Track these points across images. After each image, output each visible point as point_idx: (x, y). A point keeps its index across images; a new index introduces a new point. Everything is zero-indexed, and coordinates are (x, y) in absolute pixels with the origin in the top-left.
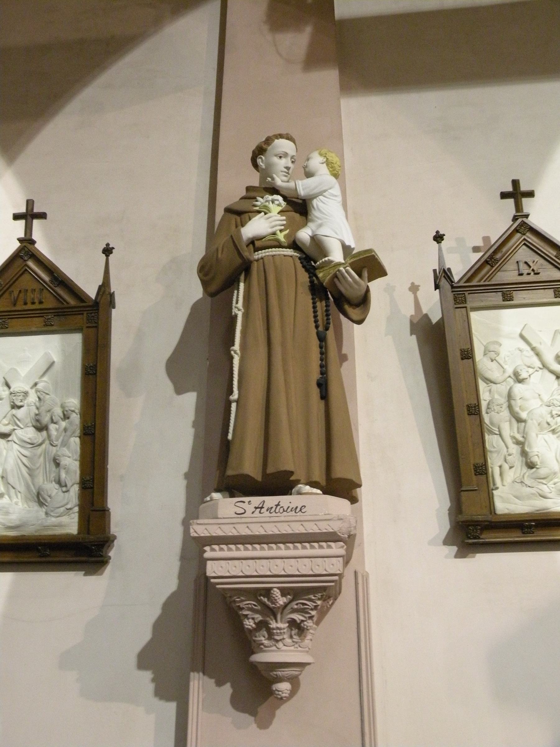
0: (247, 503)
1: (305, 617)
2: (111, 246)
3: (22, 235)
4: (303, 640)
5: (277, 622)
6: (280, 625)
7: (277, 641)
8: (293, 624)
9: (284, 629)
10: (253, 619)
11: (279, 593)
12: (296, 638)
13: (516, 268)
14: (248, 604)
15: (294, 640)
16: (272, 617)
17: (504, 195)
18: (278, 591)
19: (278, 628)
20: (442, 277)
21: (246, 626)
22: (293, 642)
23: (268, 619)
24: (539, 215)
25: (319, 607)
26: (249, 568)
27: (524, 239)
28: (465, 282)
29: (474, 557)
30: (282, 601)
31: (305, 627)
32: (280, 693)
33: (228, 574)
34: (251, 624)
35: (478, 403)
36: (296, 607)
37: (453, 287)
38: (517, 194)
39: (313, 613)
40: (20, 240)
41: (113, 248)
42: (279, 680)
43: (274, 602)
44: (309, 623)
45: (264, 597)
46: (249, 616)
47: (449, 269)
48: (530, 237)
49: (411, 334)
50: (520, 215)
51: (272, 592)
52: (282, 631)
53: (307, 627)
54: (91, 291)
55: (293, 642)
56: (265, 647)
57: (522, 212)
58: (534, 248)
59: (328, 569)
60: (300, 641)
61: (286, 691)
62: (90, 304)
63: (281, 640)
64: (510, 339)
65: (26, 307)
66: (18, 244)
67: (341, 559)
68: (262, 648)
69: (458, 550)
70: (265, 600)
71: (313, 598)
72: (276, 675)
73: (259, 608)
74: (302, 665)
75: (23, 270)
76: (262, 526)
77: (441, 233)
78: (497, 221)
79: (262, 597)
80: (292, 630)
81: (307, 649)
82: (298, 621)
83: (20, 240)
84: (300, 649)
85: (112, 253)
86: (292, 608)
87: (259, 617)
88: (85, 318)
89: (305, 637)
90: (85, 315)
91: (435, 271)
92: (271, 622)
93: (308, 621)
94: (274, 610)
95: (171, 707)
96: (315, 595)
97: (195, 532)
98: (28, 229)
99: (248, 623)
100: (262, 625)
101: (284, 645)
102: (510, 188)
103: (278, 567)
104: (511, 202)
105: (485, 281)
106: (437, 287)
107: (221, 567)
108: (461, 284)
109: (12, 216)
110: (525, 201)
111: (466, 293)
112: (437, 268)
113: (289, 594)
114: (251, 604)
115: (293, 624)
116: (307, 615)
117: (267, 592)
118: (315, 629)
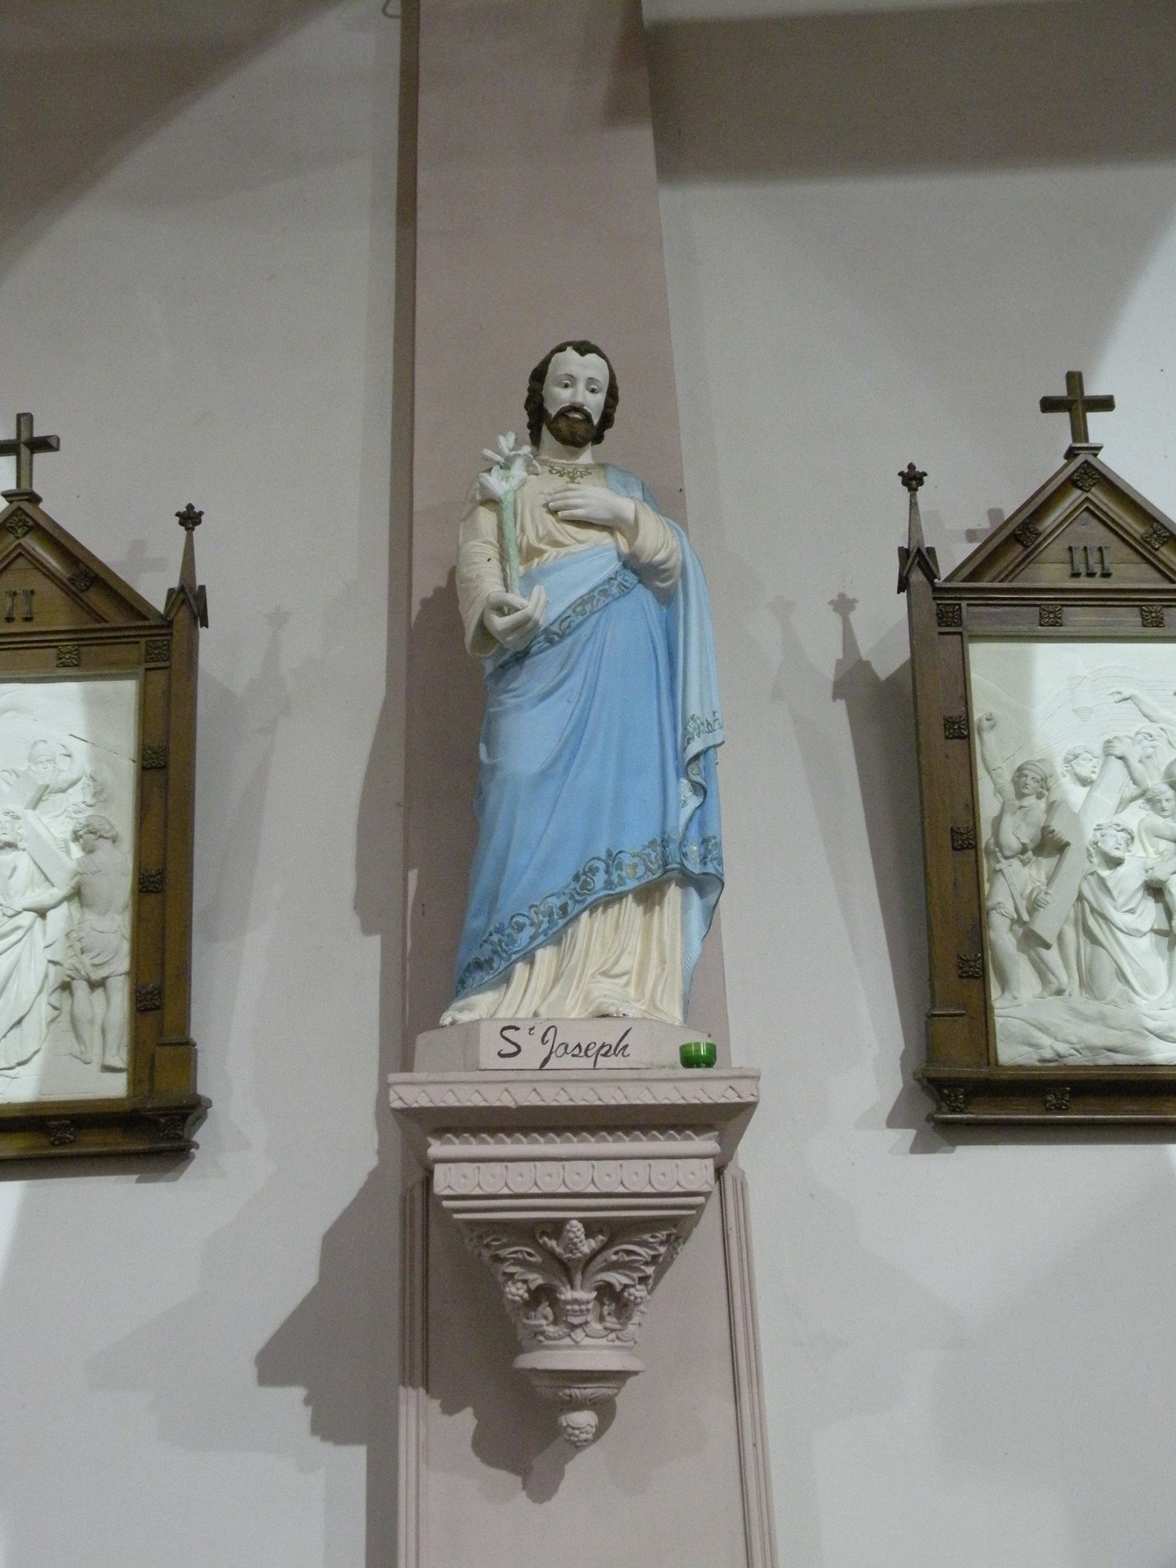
1: (633, 1280)
2: (197, 510)
3: (12, 486)
4: (624, 1325)
5: (573, 1287)
7: (573, 1327)
8: (606, 1292)
9: (588, 1302)
10: (525, 1282)
12: (611, 1322)
13: (1068, 559)
15: (608, 1325)
16: (564, 1279)
17: (1049, 405)
18: (580, 1226)
19: (575, 1301)
20: (916, 561)
21: (510, 1296)
22: (606, 1329)
23: (557, 1283)
25: (661, 1259)
26: (521, 1179)
27: (1087, 499)
28: (964, 581)
29: (952, 1151)
30: (587, 1246)
31: (632, 1298)
32: (577, 1432)
33: (478, 1192)
34: (521, 1292)
36: (614, 1258)
37: (936, 589)
39: (650, 1270)
40: (7, 495)
41: (201, 513)
42: (576, 1405)
43: (571, 1246)
44: (639, 1292)
47: (931, 551)
48: (1098, 495)
49: (835, 697)
51: (568, 1227)
52: (583, 1307)
53: (636, 1298)
55: (606, 1329)
56: (548, 1338)
57: (1087, 440)
58: (1100, 515)
59: (683, 1183)
60: (618, 1327)
61: (589, 1428)
62: (158, 622)
63: (580, 1325)
64: (1071, 708)
65: (12, 628)
68: (540, 1341)
70: (552, 1243)
71: (651, 1240)
72: (570, 1396)
73: (537, 1259)
74: (619, 1377)
76: (535, 1090)
77: (919, 469)
79: (546, 1239)
80: (602, 1304)
81: (631, 1344)
82: (618, 1288)
83: (7, 495)
84: (617, 1343)
85: (200, 522)
86: (606, 1261)
87: (536, 1279)
88: (143, 650)
89: (629, 1318)
92: (562, 1289)
93: (638, 1287)
94: (570, 1265)
95: (355, 1457)
96: (646, 1234)
97: (400, 1098)
99: (513, 1290)
100: (541, 1295)
101: (587, 1335)
102: (1060, 390)
103: (579, 1177)
104: (1062, 419)
105: (1002, 581)
107: (470, 1175)
110: (1094, 419)
111: (964, 604)
113: (601, 1232)
114: (521, 1252)
115: (606, 1292)
116: (636, 1275)
117: (557, 1228)
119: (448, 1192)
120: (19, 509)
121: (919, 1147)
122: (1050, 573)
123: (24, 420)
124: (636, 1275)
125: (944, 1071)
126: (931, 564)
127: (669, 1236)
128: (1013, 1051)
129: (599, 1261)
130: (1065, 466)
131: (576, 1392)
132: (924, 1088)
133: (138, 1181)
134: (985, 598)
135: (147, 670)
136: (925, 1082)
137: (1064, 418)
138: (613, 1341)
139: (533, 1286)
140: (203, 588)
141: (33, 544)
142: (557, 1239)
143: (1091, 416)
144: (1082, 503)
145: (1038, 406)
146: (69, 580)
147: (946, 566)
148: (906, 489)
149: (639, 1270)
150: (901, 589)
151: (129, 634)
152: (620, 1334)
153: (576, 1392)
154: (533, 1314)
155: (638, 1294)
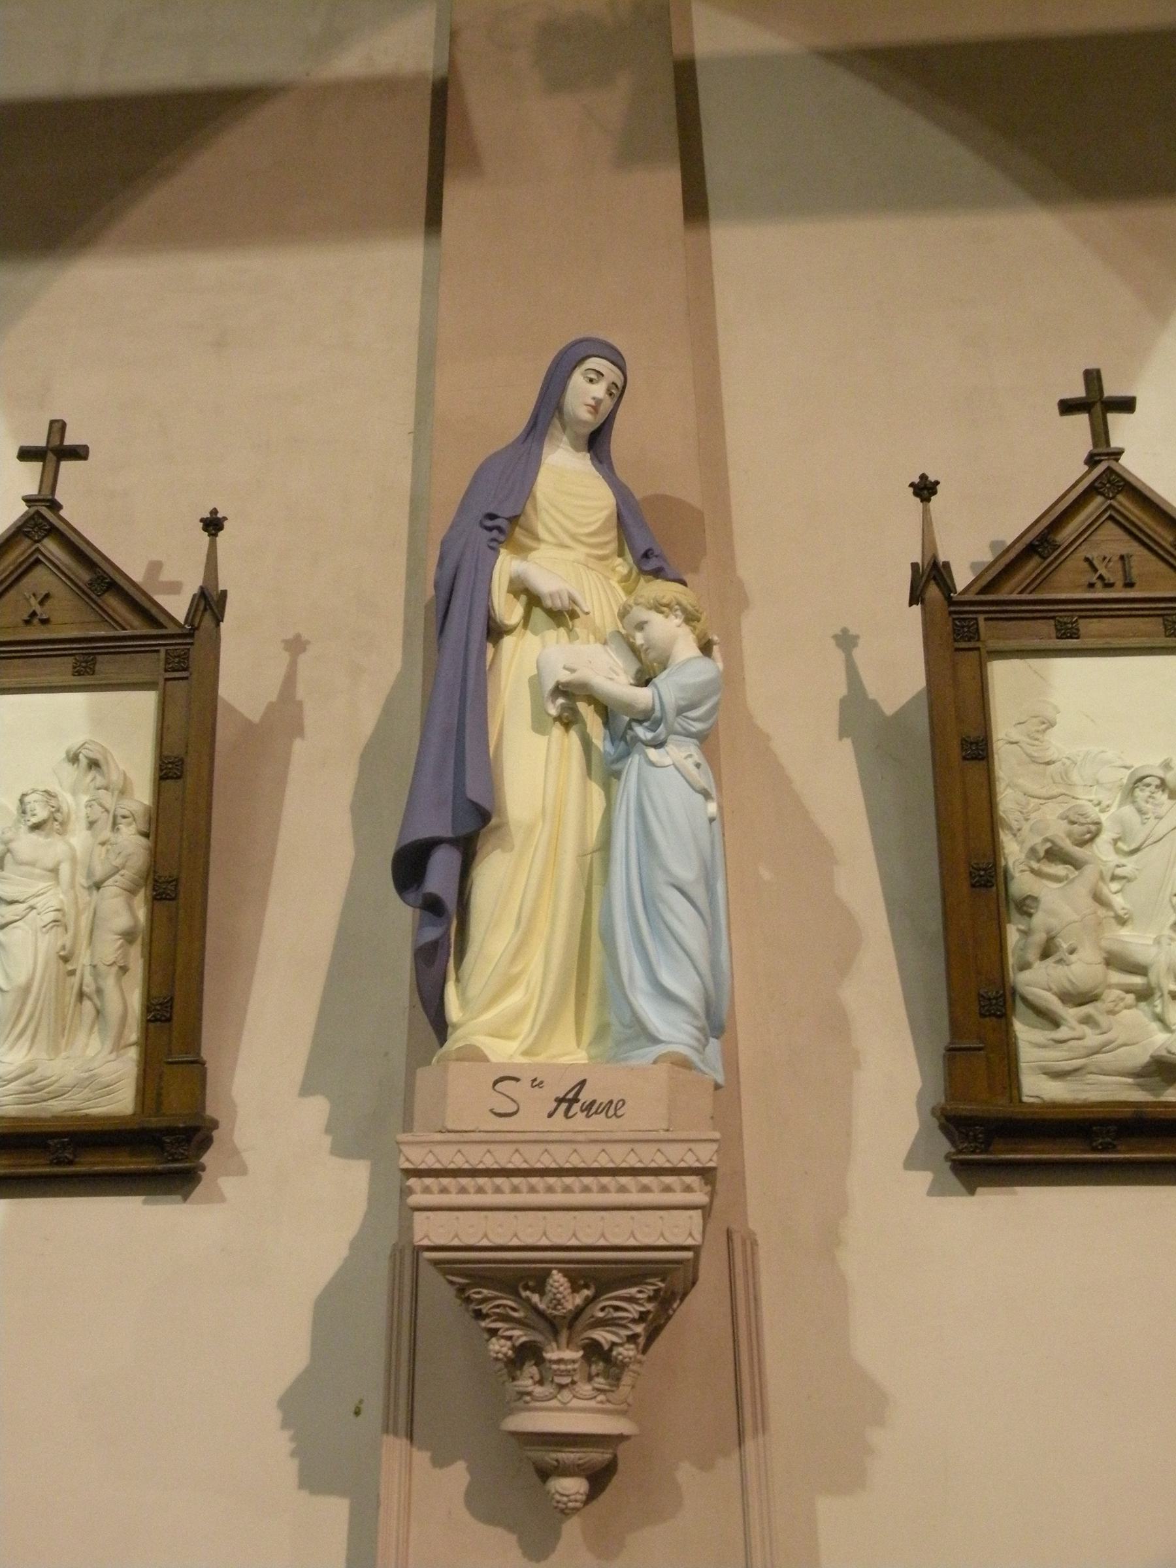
0: (526, 1083)
2: (219, 516)
3: (32, 490)
6: (568, 1354)
7: (561, 1387)
10: (510, 1338)
11: (567, 1285)
12: (600, 1382)
14: (498, 1306)
15: (597, 1386)
17: (1068, 407)
18: (563, 1280)
20: (930, 577)
24: (81, 500)
25: (651, 1316)
27: (1110, 507)
28: (978, 594)
30: (574, 1301)
31: (620, 1357)
32: (565, 1499)
34: (504, 1350)
35: (995, 859)
36: (601, 1315)
37: (951, 602)
38: (1097, 403)
39: (639, 1329)
40: (28, 500)
45: (533, 1291)
46: (500, 1333)
47: (947, 565)
50: (1102, 453)
54: (178, 607)
56: (535, 1399)
66: (23, 508)
67: (699, 1212)
69: (933, 1180)
70: (535, 1298)
72: (557, 1461)
75: (32, 560)
77: (932, 478)
78: (1056, 461)
81: (624, 1407)
82: (606, 1347)
83: (28, 500)
84: (609, 1406)
87: (521, 1336)
90: (162, 655)
91: (914, 566)
93: (627, 1346)
95: (335, 1511)
98: (50, 480)
101: (574, 1396)
105: (1021, 592)
106: (915, 598)
108: (970, 597)
109: (15, 452)
111: (981, 618)
112: (920, 562)
113: (586, 1286)
114: (505, 1306)
115: (594, 1351)
116: (625, 1333)
118: (640, 1362)
119: (426, 1242)
120: (38, 513)
121: (936, 1190)
122: (1068, 584)
123: (58, 427)
124: (625, 1333)
125: (964, 1108)
126: (949, 581)
127: (657, 1291)
128: (1037, 1088)
129: (585, 1319)
130: (1088, 473)
131: (562, 1456)
132: (943, 1128)
133: (145, 1202)
134: (1007, 612)
135: (167, 680)
136: (943, 1120)
137: (1083, 419)
138: (601, 1402)
139: (518, 1343)
140: (224, 593)
141: (51, 547)
142: (542, 1293)
143: (1112, 417)
144: (1105, 511)
145: (1056, 411)
146: (91, 584)
147: (962, 578)
148: (918, 500)
149: (625, 1327)
150: (913, 601)
151: (154, 642)
152: (611, 1396)
153: (562, 1456)
154: (518, 1373)
155: (625, 1353)
